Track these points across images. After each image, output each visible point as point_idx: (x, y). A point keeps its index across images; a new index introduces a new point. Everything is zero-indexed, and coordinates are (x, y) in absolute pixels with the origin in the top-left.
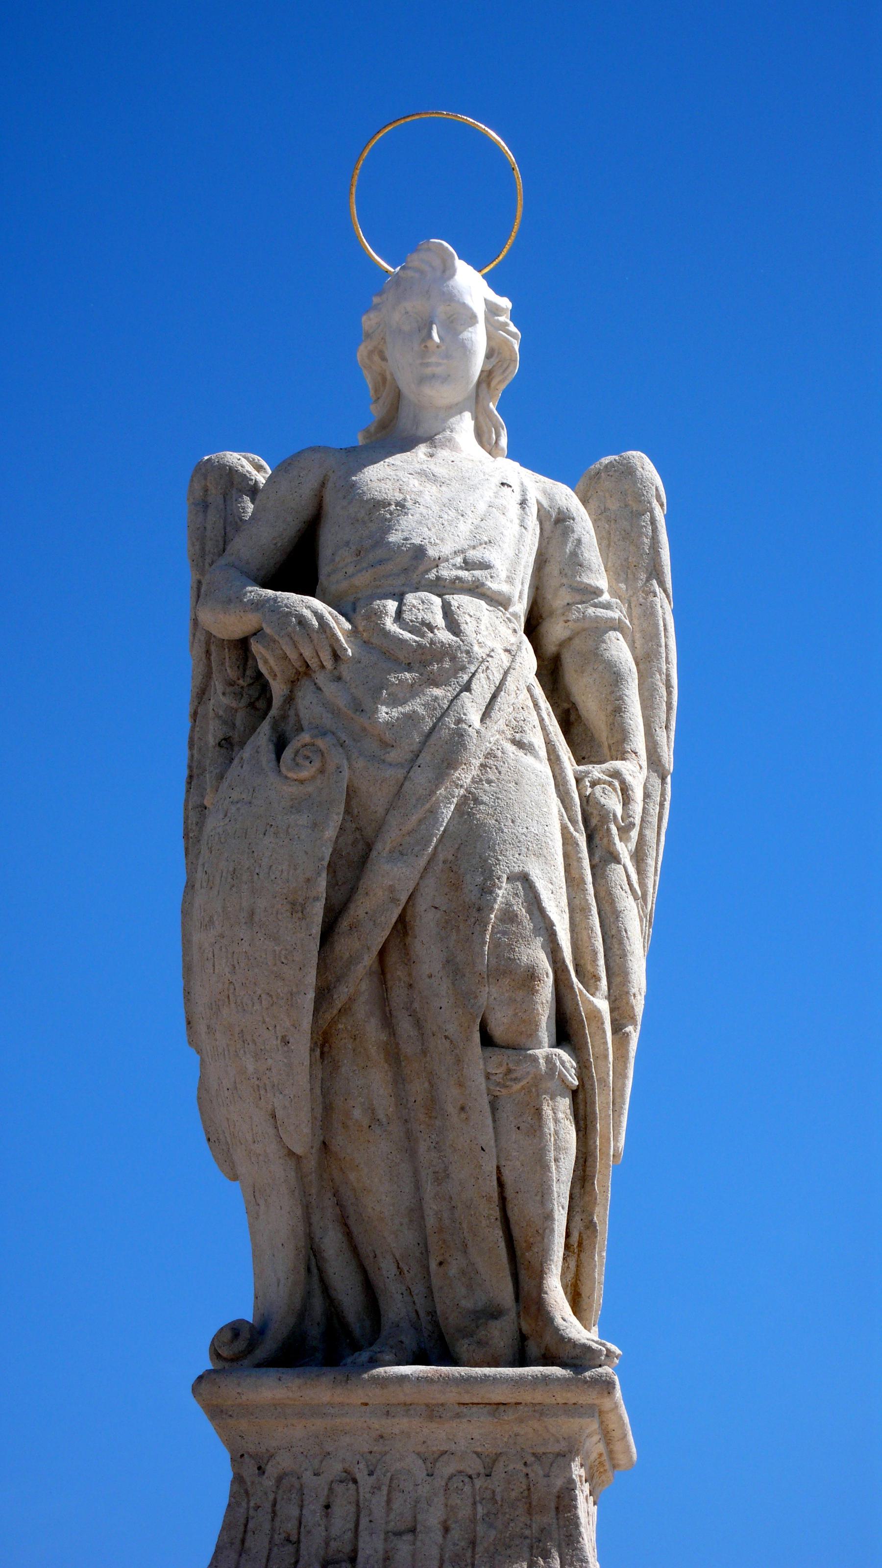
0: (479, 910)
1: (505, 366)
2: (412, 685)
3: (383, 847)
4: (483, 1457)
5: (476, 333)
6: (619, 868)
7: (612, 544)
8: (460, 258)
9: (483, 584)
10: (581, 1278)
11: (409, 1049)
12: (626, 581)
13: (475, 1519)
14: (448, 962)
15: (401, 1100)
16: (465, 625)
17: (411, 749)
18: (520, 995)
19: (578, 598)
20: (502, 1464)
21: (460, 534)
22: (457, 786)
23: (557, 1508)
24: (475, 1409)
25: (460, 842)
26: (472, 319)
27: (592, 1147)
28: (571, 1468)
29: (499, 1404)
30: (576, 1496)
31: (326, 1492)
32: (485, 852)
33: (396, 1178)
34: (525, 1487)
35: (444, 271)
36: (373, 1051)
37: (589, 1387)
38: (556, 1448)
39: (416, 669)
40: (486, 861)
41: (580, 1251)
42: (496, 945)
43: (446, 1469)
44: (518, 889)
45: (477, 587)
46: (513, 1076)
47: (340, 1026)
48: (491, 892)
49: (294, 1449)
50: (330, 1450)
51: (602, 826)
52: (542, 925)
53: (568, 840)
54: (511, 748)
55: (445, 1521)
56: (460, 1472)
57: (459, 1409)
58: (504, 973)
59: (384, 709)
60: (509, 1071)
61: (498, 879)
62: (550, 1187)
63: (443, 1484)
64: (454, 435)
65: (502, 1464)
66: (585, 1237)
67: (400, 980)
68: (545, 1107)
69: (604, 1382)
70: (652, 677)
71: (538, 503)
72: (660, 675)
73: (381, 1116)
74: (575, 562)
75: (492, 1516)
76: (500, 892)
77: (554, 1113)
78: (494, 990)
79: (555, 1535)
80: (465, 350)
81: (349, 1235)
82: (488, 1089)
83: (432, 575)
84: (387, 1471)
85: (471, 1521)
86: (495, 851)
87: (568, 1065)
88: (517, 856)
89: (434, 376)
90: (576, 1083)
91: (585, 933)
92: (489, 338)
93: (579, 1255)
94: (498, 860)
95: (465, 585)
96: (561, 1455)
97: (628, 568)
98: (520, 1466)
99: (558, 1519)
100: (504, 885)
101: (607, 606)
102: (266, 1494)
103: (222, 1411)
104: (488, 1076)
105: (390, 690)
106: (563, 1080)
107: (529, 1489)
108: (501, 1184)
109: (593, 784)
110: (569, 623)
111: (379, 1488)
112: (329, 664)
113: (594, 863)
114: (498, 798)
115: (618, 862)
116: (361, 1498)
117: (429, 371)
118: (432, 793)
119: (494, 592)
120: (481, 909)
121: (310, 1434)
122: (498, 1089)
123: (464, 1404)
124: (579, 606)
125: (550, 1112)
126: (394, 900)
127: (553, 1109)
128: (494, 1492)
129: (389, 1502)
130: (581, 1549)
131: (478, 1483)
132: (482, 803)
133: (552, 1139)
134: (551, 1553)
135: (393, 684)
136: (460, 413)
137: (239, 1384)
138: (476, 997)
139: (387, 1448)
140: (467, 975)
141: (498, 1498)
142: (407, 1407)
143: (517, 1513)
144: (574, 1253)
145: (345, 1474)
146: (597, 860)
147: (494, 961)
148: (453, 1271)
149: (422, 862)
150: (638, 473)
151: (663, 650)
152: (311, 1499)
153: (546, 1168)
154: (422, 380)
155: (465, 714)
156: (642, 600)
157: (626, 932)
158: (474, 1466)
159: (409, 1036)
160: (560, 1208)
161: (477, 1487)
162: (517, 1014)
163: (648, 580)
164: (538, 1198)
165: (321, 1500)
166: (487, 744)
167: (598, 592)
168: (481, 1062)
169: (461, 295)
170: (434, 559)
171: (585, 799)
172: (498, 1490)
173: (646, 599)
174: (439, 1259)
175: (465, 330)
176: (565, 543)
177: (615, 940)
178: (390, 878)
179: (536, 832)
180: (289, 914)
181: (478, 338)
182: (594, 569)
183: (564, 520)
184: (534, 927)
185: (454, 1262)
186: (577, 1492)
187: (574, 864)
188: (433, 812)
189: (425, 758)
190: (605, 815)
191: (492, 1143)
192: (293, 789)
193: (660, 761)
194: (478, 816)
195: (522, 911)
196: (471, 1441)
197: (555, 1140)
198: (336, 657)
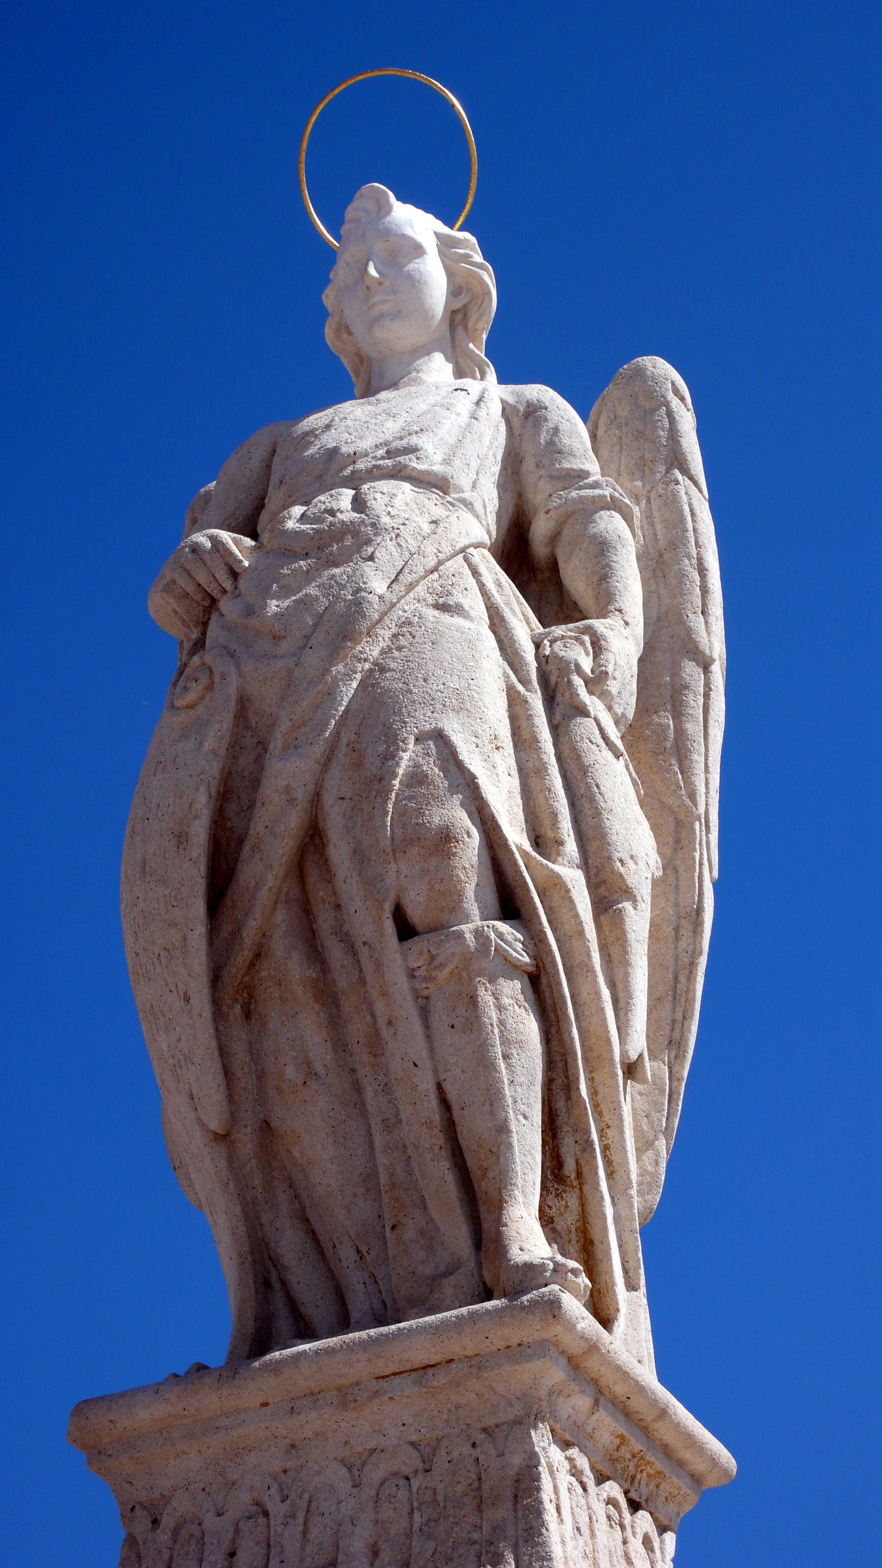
0: (380, 780)
1: (479, 302)
3: (276, 743)
4: (422, 1447)
5: (424, 264)
6: (590, 723)
7: (625, 447)
8: (401, 198)
9: (406, 466)
10: (590, 1220)
11: (343, 981)
12: (642, 478)
13: (411, 1532)
14: (355, 852)
16: (373, 502)
17: (304, 633)
18: (433, 862)
19: (560, 485)
20: (443, 1451)
21: (385, 431)
22: (359, 660)
23: (516, 1497)
24: (397, 1380)
25: (361, 717)
26: (418, 250)
27: (569, 1042)
29: (425, 1368)
30: (539, 1473)
31: (231, 1534)
32: (389, 719)
33: (342, 1140)
35: (379, 211)
36: (299, 991)
37: (527, 1313)
39: (313, 555)
40: (390, 728)
42: (401, 812)
43: (375, 1474)
44: (429, 748)
45: (400, 471)
48: (393, 757)
49: (192, 1486)
50: (235, 1477)
51: (562, 680)
52: (461, 781)
54: (431, 614)
55: (375, 1543)
56: (395, 1474)
57: (376, 1385)
58: (412, 842)
59: (275, 602)
61: (403, 741)
63: (373, 1493)
64: (420, 375)
66: (582, 1162)
67: (324, 901)
68: (481, 992)
69: (546, 1302)
70: (679, 564)
71: (502, 401)
72: (689, 560)
73: (319, 1068)
74: (554, 449)
75: (433, 1524)
77: (496, 999)
78: (403, 866)
81: (312, 1233)
82: (414, 990)
84: (303, 1491)
86: (401, 714)
87: (509, 938)
88: (429, 714)
89: (382, 315)
90: (526, 959)
91: (541, 796)
92: (450, 274)
93: (581, 1190)
94: (405, 723)
95: (385, 471)
96: (517, 1422)
97: (645, 465)
98: (467, 1449)
99: (515, 1511)
101: (596, 485)
102: (160, 1552)
104: (411, 974)
105: (281, 583)
106: (506, 958)
107: (480, 1479)
108: (445, 1103)
109: (552, 642)
110: (551, 513)
111: (293, 1516)
112: (228, 585)
113: (555, 722)
114: (408, 661)
115: (587, 715)
116: (272, 1533)
117: (376, 311)
118: (327, 671)
119: (422, 472)
120: (383, 779)
121: (208, 1461)
122: (424, 985)
123: (383, 1377)
124: (562, 493)
125: (490, 999)
126: (292, 801)
127: (493, 994)
128: (435, 1491)
130: (544, 1544)
131: (415, 1483)
132: (390, 670)
133: (496, 1031)
134: (503, 1556)
136: (429, 354)
137: (110, 1409)
138: (383, 880)
139: (303, 1460)
140: (373, 858)
141: (440, 1498)
142: (314, 1395)
143: (463, 1513)
144: (573, 1187)
145: (256, 1507)
146: (558, 717)
147: (399, 832)
148: (410, 1233)
149: (318, 750)
150: (648, 373)
151: (691, 534)
152: (212, 1548)
153: (491, 1067)
154: (372, 323)
155: (365, 583)
156: (661, 491)
157: (598, 786)
158: (410, 1461)
159: (343, 966)
160: (521, 1117)
161: (415, 1489)
162: (432, 887)
163: (668, 471)
164: (487, 1108)
165: (224, 1547)
166: (401, 613)
167: (583, 474)
169: (400, 228)
170: (349, 455)
171: (543, 660)
172: (441, 1486)
173: (666, 489)
174: (393, 1222)
175: (410, 262)
177: (584, 799)
178: (287, 776)
179: (457, 686)
180: (175, 849)
181: (433, 273)
182: (578, 454)
183: (535, 411)
184: (450, 785)
185: (411, 1222)
186: (540, 1468)
187: (524, 723)
188: (331, 694)
189: (319, 637)
190: (566, 668)
191: (425, 1053)
192: (183, 718)
193: (697, 648)
194: (382, 685)
195: (433, 770)
196: (402, 1428)
197: (501, 1032)
198: (234, 575)
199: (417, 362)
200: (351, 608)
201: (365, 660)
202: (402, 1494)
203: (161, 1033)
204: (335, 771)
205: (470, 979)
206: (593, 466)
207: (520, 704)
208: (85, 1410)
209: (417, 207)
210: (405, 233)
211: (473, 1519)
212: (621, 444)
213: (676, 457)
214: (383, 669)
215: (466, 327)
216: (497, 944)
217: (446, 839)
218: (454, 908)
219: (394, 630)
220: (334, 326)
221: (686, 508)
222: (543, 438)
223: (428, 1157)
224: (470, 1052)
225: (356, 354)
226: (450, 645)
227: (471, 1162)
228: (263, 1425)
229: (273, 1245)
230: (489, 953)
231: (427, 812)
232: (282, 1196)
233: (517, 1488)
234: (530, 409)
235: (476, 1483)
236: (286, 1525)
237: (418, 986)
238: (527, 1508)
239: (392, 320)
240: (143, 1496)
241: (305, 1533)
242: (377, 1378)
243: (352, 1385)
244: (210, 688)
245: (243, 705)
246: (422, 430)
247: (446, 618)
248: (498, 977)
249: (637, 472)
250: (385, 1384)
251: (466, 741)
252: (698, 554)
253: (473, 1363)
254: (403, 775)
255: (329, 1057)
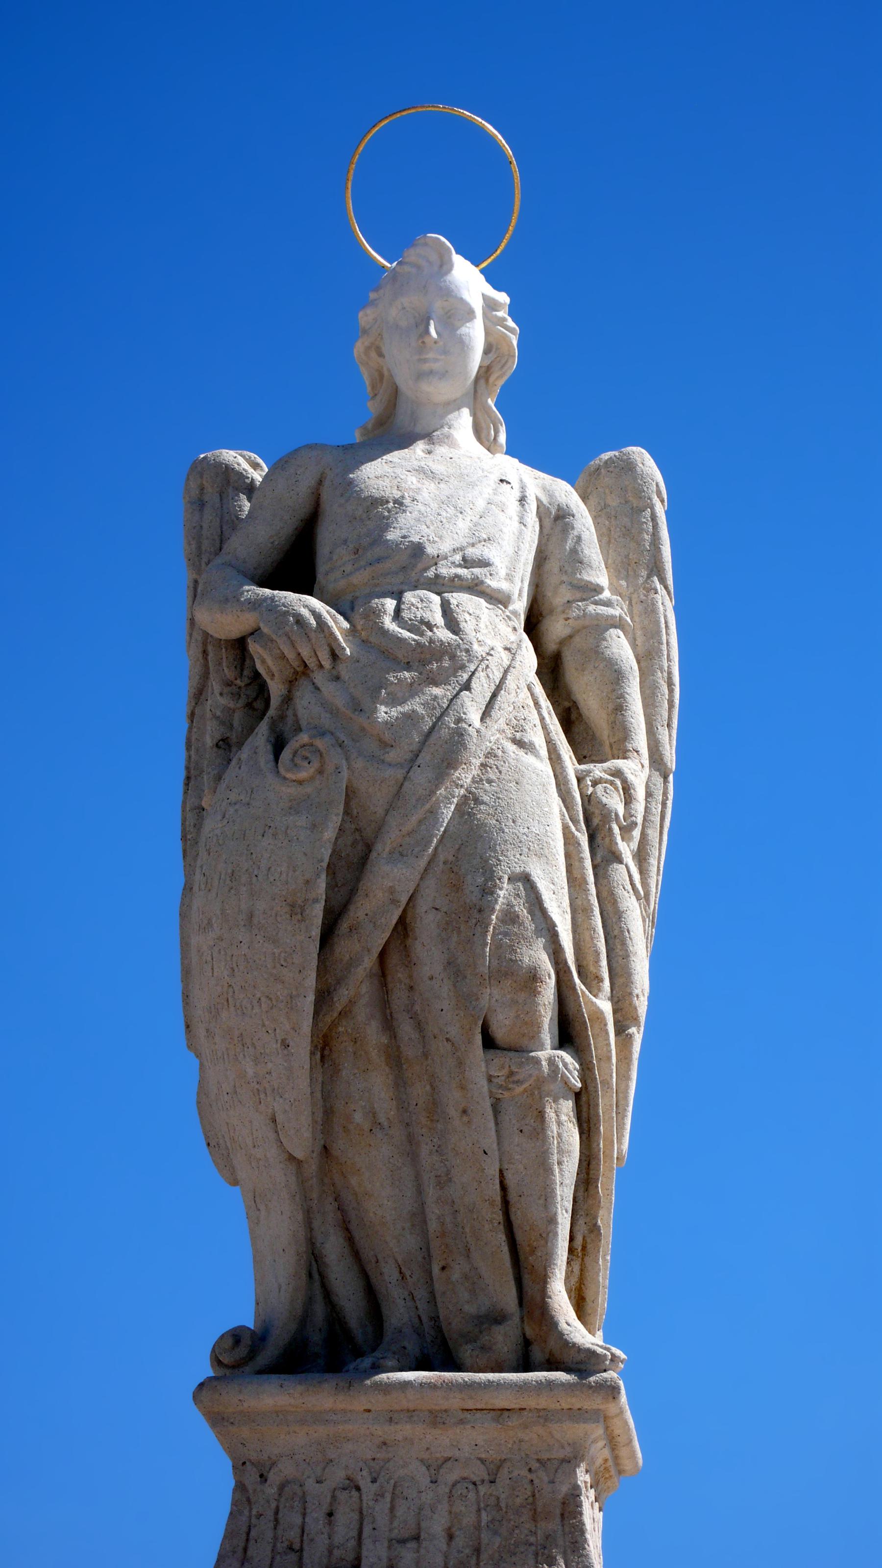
0: (480, 911)
1: (503, 361)
2: (411, 684)
3: (383, 848)
6: (621, 868)
7: (613, 541)
8: (457, 253)
9: (482, 582)
11: (410, 1051)
12: (627, 578)
14: (449, 963)
15: (402, 1104)
16: (464, 624)
18: (522, 996)
19: (578, 595)
20: (506, 1470)
22: (457, 786)
23: (562, 1515)
24: (479, 1415)
25: (460, 842)
28: (576, 1474)
29: (503, 1410)
30: (581, 1502)
31: (328, 1499)
32: (485, 853)
34: (529, 1494)
35: (441, 266)
36: (374, 1054)
37: (593, 1392)
38: (561, 1454)
39: (415, 668)
40: (487, 861)
41: (584, 1255)
42: (498, 946)
45: (476, 585)
46: (516, 1078)
47: (341, 1029)
48: (492, 893)
49: (296, 1457)
50: (332, 1457)
51: (604, 826)
52: (544, 926)
53: (569, 840)
54: (511, 748)
55: (450, 1528)
56: (464, 1479)
58: (506, 975)
59: (383, 708)
60: (511, 1074)
61: (499, 879)
62: (553, 1191)
64: (452, 431)
65: (506, 1470)
66: (589, 1240)
67: (401, 982)
68: (548, 1110)
69: (609, 1386)
70: (653, 675)
72: (662, 673)
73: (382, 1119)
74: (576, 559)
76: (501, 893)
77: (557, 1116)
79: (560, 1542)
80: (463, 346)
81: (350, 1240)
82: (490, 1092)
83: (431, 573)
84: (390, 1478)
85: (475, 1528)
86: (495, 851)
87: (571, 1067)
88: (518, 856)
89: (431, 372)
90: (579, 1085)
91: (587, 934)
92: (487, 333)
93: (583, 1259)
94: (499, 860)
95: (464, 583)
96: (566, 1461)
98: (524, 1472)
99: (563, 1526)
100: (505, 885)
101: (608, 604)
102: (268, 1502)
103: (223, 1419)
104: (490, 1079)
105: (389, 690)
106: (566, 1083)
107: (534, 1496)
108: (504, 1188)
109: (595, 783)
111: (382, 1496)
112: (327, 663)
113: (596, 862)
114: (499, 798)
117: (426, 367)
118: (432, 793)
119: (494, 590)
120: (482, 910)
122: (500, 1091)
123: (467, 1410)
124: (580, 603)
125: (553, 1115)
126: (394, 902)
127: (556, 1112)
128: (498, 1498)
129: (392, 1509)
130: (587, 1556)
131: (483, 1490)
132: (483, 803)
133: (555, 1142)
135: (392, 683)
137: (240, 1392)
138: (477, 999)
141: (503, 1505)
142: (410, 1414)
143: (522, 1520)
144: (578, 1257)
145: (348, 1482)
146: (598, 859)
147: (495, 963)
149: (423, 863)
150: (638, 469)
151: (664, 647)
152: (314, 1507)
153: (549, 1171)
154: (420, 376)
155: (465, 713)
156: (643, 597)
158: (479, 1472)
161: (482, 1493)
163: (649, 576)
164: (541, 1202)
166: (488, 744)
167: (598, 589)
168: (483, 1064)
171: (586, 799)
172: (503, 1496)
174: (442, 1263)
176: (564, 540)
177: (617, 941)
178: (390, 880)
179: (537, 832)
180: (288, 916)
181: (476, 334)
182: (594, 566)
183: (564, 517)
184: (536, 927)
185: (457, 1266)
186: (582, 1498)
188: (433, 813)
189: (425, 757)
190: (607, 815)
191: (495, 1146)
192: (292, 790)
193: (662, 760)
194: (478, 816)
195: (523, 912)
196: (475, 1447)
197: (558, 1143)
198: (335, 655)
199: (449, 416)
200: (454, 737)
201: (462, 786)
202: (472, 1495)
203: (248, 1059)
204: (431, 883)
205: (541, 1098)
206: (601, 578)
207: (574, 845)
208: (218, 1387)
209: (466, 258)
210: (464, 297)
211: (529, 1525)
212: (609, 536)
213: (655, 563)
214: (477, 801)
215: (487, 381)
216: (563, 1072)
217: (533, 978)
218: (535, 1036)
219: (482, 759)
220: (367, 344)
221: (662, 620)
222: (569, 544)
223: (487, 1227)
224: (534, 1155)
225: (377, 370)
226: (530, 788)
227: (519, 1237)
228: (365, 1426)
229: (318, 1245)
230: (557, 1080)
231: (518, 950)
232: (330, 1207)
233: (563, 1509)
234: (561, 513)
235: (531, 1499)
236: (376, 1500)
237: (494, 1090)
238: (573, 1526)
239: (440, 379)
240: (253, 1456)
241: (392, 1509)
242: (463, 1410)
243: (441, 1411)
244: (321, 772)
245: (350, 794)
246: (489, 539)
247: (521, 753)
248: (559, 1098)
249: (622, 571)
250: (469, 1416)
251: (547, 888)
252: (669, 667)
253: (541, 1414)
254: (499, 911)
255: (392, 1113)
